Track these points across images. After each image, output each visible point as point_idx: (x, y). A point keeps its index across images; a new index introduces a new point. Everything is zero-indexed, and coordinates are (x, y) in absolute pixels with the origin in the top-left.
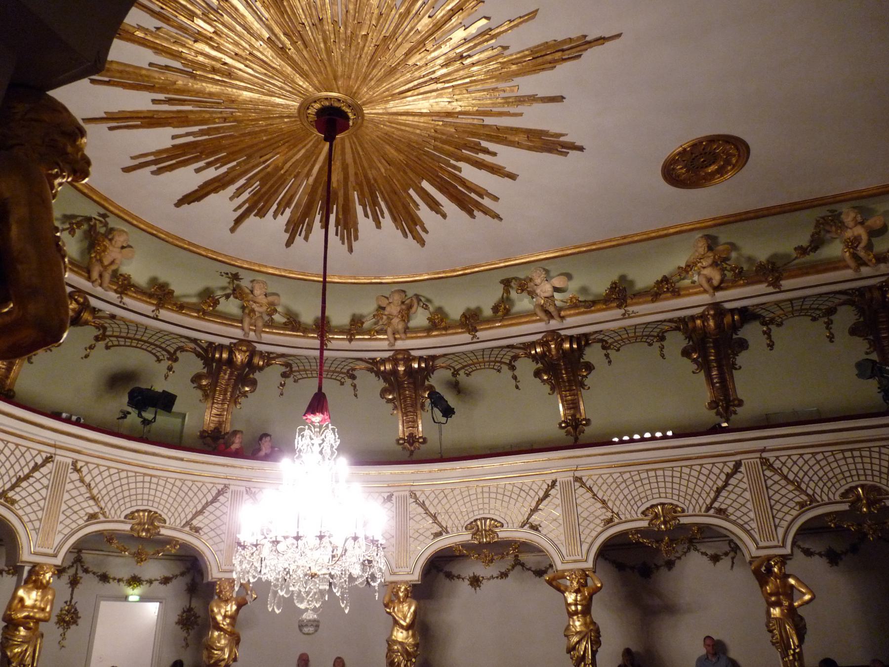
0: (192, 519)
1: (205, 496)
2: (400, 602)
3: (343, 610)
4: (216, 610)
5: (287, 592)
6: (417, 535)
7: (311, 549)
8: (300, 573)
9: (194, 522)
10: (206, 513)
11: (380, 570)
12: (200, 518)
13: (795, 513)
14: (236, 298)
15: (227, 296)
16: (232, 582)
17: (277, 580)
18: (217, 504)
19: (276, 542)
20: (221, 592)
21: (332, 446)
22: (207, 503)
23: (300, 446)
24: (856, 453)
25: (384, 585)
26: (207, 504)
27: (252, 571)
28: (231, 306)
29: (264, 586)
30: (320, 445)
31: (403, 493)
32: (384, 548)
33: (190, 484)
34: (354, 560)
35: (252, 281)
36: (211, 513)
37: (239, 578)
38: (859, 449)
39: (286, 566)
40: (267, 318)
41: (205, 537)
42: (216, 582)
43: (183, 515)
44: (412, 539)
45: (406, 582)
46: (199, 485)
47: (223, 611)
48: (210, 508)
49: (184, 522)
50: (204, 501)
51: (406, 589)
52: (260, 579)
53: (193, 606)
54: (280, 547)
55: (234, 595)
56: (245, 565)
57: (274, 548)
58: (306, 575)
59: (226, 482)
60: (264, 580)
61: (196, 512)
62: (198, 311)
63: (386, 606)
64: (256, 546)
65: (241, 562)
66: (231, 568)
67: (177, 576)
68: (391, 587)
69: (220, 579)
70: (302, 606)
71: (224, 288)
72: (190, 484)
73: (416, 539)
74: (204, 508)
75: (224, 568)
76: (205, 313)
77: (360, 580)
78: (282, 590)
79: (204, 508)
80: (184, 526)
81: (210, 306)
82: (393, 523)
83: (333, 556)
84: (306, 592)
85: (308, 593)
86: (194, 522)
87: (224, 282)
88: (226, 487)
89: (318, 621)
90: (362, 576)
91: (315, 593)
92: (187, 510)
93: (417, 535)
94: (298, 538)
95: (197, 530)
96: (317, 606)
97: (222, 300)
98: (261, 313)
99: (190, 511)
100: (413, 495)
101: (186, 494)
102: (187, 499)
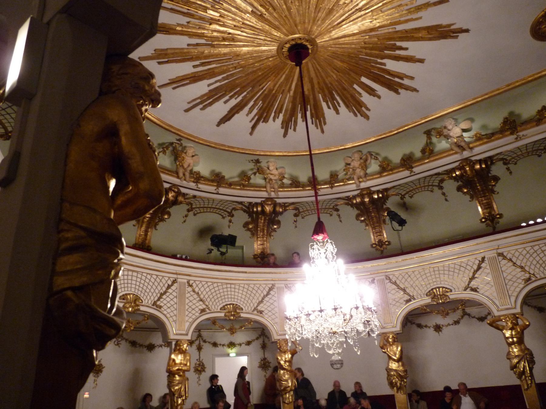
0: (257, 306)
1: (262, 292)
2: (391, 345)
3: (356, 352)
4: (279, 358)
5: (320, 344)
7: (331, 317)
8: (326, 332)
9: (259, 308)
10: (265, 302)
12: (262, 305)
13: (197, 314)
14: (260, 174)
15: (255, 174)
16: (286, 341)
18: (269, 296)
19: (308, 315)
20: (280, 347)
21: (332, 253)
24: (135, 274)
26: (265, 296)
27: (297, 333)
28: (258, 180)
29: (306, 342)
34: (358, 321)
35: (268, 162)
37: (290, 338)
38: (137, 272)
39: (317, 328)
40: (280, 182)
41: (266, 316)
43: (252, 305)
45: (392, 333)
46: (197, 283)
47: (284, 358)
48: (266, 299)
49: (253, 309)
50: (262, 295)
51: (393, 337)
52: (302, 338)
53: (266, 357)
54: (312, 317)
56: (293, 330)
58: (330, 333)
59: (273, 282)
62: (240, 185)
64: (297, 318)
65: (290, 329)
66: (284, 332)
67: (254, 340)
69: (279, 340)
70: (331, 352)
71: (252, 169)
72: (252, 286)
74: (263, 299)
76: (244, 186)
79: (263, 299)
80: (254, 311)
81: (246, 181)
83: (345, 320)
84: (332, 343)
85: (333, 344)
86: (259, 308)
87: (252, 165)
89: (342, 361)
91: (337, 344)
92: (254, 301)
94: (321, 311)
95: (261, 312)
96: (340, 351)
97: (252, 176)
98: (276, 180)
99: (255, 302)
100: (388, 278)
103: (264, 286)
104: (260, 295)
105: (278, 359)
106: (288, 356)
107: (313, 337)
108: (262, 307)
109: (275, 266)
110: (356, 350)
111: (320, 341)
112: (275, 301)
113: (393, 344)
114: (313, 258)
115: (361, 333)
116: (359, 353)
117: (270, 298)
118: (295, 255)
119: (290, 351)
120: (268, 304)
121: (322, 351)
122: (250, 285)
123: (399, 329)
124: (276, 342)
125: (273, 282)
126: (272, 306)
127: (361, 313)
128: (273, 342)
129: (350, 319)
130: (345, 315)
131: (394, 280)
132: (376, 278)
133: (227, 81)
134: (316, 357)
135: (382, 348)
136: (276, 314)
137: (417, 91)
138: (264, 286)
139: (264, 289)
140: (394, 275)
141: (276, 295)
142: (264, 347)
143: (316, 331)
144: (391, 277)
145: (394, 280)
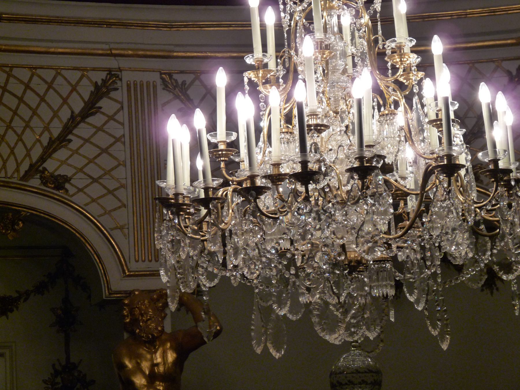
0: (43, 159)
1: (65, 101)
3: (435, 342)
4: (129, 364)
5: (295, 307)
7: (343, 203)
9: (50, 165)
10: (76, 143)
12: (62, 154)
16: (159, 297)
17: (267, 281)
18: (97, 120)
19: (251, 192)
20: (135, 321)
22: (73, 117)
26: (74, 121)
27: (204, 262)
29: (240, 295)
33: (24, 75)
34: (452, 220)
36: (87, 141)
37: (176, 288)
39: (285, 245)
43: (20, 151)
46: (49, 75)
47: (145, 366)
48: (83, 130)
49: (25, 167)
50: (65, 114)
52: (225, 280)
53: (74, 359)
54: (267, 202)
56: (186, 251)
57: (250, 207)
58: (335, 265)
59: (112, 63)
60: (234, 283)
61: (51, 142)
64: (205, 202)
65: (175, 244)
66: (153, 265)
67: (27, 295)
69: (129, 294)
70: (334, 339)
72: (24, 75)
74: (68, 129)
75: (134, 266)
77: (470, 273)
78: (281, 305)
79: (68, 129)
80: (27, 176)
82: (479, 100)
83: (398, 218)
85: (345, 308)
86: (50, 165)
88: (113, 75)
89: (378, 372)
90: (475, 261)
91: (363, 308)
92: (29, 138)
94: (306, 176)
95: (59, 183)
96: (372, 336)
99: (35, 140)
101: (21, 100)
102: (25, 112)
104: (56, 114)
105: (123, 366)
106: (165, 357)
108: (63, 162)
110: (435, 333)
112: (117, 140)
116: (445, 346)
117: (100, 129)
121: (300, 333)
122: (16, 72)
127: (464, 192)
128: (103, 304)
129: (419, 215)
130: (401, 196)
134: (277, 355)
137: (81, 360)
138: (74, 76)
142: (66, 322)
143: (281, 254)
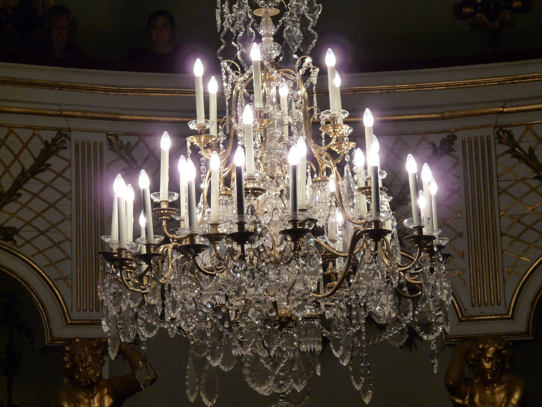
1: (16, 157)
2: (486, 383)
3: (358, 396)
5: (228, 359)
6: (517, 229)
7: (276, 263)
8: (253, 317)
10: (25, 197)
11: (441, 305)
16: (101, 345)
17: (201, 334)
18: (45, 176)
19: (191, 249)
20: (75, 368)
21: (304, 23)
22: (23, 173)
23: (226, 25)
25: (446, 341)
26: (24, 177)
29: (175, 348)
30: (275, 19)
31: (478, 133)
32: (446, 256)
34: (378, 282)
36: (35, 195)
37: (116, 338)
39: (220, 300)
41: (28, 250)
42: (61, 347)
44: (506, 240)
45: (497, 338)
48: (32, 185)
50: (16, 170)
51: (497, 353)
52: (163, 331)
54: (205, 259)
55: (106, 375)
56: (128, 304)
58: (267, 320)
59: (61, 123)
63: (454, 391)
64: (147, 258)
65: (117, 297)
66: (94, 315)
68: (463, 349)
69: (70, 341)
70: (264, 390)
73: (517, 238)
74: (19, 184)
75: (75, 315)
77: (394, 331)
79: (19, 184)
83: (327, 278)
84: (270, 358)
85: (275, 361)
88: (62, 135)
90: (397, 321)
91: (291, 362)
93: (517, 229)
94: (242, 236)
96: (299, 389)
100: (504, 135)
103: (25, 134)
107: (201, 334)
109: (78, 58)
110: (358, 387)
111: (228, 349)
112: (64, 195)
113: (496, 380)
114: (229, 36)
115: (382, 328)
116: (367, 401)
117: (48, 185)
118: (160, 21)
119: (110, 384)
120: (38, 205)
123: (524, 329)
124: (60, 349)
125: (61, 123)
126: (53, 216)
129: (347, 276)
130: (330, 257)
131: (525, 147)
132: (460, 135)
133: (315, 95)
135: (454, 391)
136: (66, 246)
138: (25, 134)
139: (25, 146)
140: (529, 127)
141: (70, 174)
143: (217, 309)
144: (517, 133)
145: (525, 147)
